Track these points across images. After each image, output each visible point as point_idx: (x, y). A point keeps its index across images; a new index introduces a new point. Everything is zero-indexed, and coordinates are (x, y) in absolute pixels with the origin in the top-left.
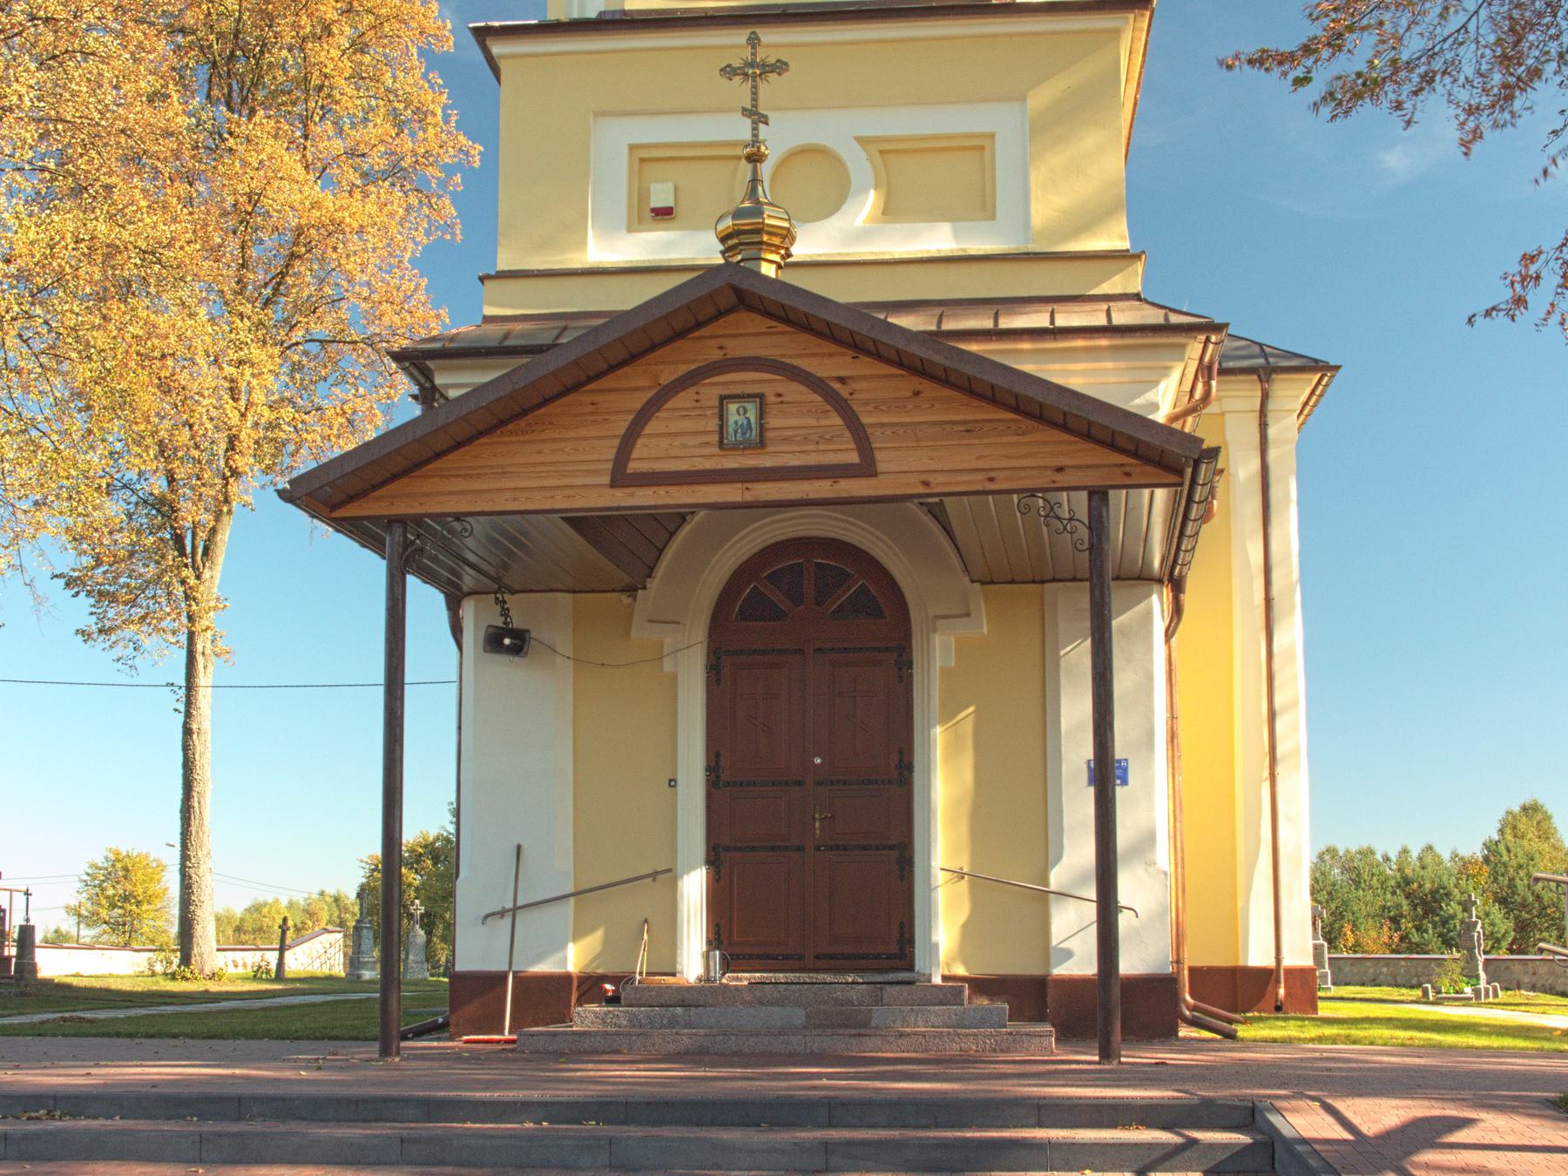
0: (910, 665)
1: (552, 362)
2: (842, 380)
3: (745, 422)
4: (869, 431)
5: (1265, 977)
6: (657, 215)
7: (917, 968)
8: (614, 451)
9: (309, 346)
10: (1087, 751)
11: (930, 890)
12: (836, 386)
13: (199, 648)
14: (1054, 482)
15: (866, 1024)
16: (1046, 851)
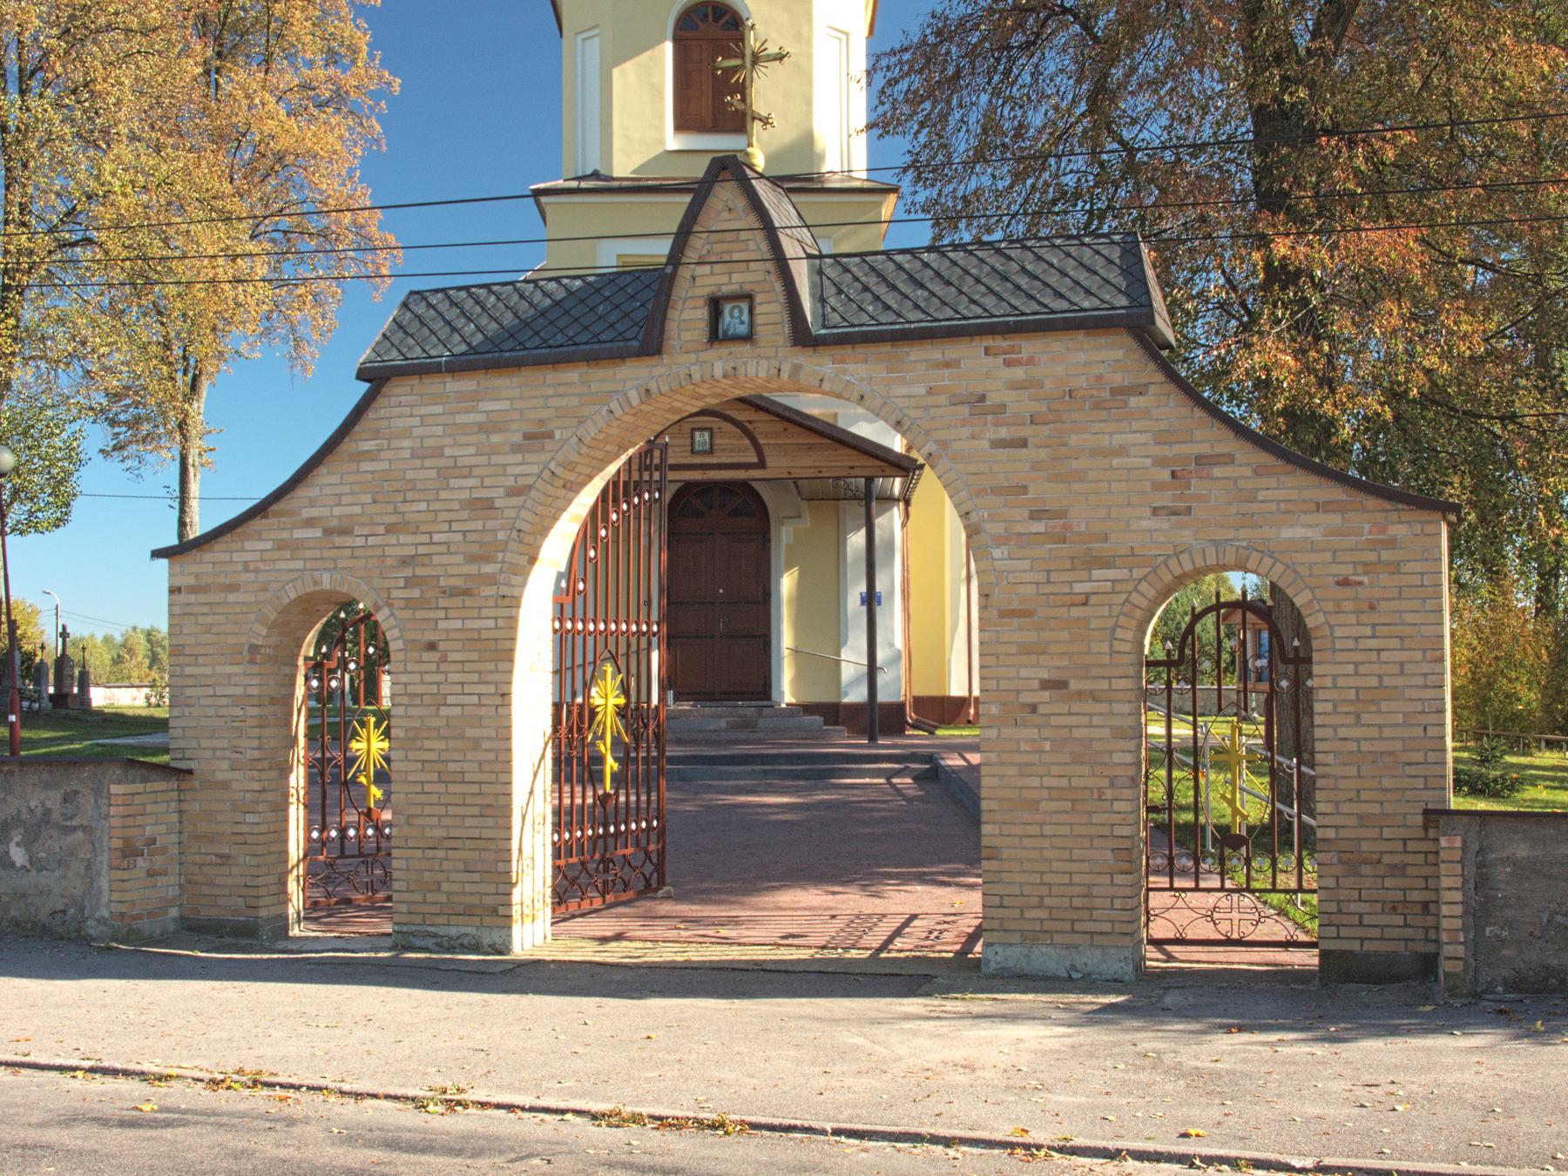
0: (769, 542)
2: (750, 422)
5: (962, 703)
9: (275, 235)
10: (863, 588)
11: (780, 659)
12: (747, 425)
13: (190, 461)
15: (755, 726)
16: (838, 642)
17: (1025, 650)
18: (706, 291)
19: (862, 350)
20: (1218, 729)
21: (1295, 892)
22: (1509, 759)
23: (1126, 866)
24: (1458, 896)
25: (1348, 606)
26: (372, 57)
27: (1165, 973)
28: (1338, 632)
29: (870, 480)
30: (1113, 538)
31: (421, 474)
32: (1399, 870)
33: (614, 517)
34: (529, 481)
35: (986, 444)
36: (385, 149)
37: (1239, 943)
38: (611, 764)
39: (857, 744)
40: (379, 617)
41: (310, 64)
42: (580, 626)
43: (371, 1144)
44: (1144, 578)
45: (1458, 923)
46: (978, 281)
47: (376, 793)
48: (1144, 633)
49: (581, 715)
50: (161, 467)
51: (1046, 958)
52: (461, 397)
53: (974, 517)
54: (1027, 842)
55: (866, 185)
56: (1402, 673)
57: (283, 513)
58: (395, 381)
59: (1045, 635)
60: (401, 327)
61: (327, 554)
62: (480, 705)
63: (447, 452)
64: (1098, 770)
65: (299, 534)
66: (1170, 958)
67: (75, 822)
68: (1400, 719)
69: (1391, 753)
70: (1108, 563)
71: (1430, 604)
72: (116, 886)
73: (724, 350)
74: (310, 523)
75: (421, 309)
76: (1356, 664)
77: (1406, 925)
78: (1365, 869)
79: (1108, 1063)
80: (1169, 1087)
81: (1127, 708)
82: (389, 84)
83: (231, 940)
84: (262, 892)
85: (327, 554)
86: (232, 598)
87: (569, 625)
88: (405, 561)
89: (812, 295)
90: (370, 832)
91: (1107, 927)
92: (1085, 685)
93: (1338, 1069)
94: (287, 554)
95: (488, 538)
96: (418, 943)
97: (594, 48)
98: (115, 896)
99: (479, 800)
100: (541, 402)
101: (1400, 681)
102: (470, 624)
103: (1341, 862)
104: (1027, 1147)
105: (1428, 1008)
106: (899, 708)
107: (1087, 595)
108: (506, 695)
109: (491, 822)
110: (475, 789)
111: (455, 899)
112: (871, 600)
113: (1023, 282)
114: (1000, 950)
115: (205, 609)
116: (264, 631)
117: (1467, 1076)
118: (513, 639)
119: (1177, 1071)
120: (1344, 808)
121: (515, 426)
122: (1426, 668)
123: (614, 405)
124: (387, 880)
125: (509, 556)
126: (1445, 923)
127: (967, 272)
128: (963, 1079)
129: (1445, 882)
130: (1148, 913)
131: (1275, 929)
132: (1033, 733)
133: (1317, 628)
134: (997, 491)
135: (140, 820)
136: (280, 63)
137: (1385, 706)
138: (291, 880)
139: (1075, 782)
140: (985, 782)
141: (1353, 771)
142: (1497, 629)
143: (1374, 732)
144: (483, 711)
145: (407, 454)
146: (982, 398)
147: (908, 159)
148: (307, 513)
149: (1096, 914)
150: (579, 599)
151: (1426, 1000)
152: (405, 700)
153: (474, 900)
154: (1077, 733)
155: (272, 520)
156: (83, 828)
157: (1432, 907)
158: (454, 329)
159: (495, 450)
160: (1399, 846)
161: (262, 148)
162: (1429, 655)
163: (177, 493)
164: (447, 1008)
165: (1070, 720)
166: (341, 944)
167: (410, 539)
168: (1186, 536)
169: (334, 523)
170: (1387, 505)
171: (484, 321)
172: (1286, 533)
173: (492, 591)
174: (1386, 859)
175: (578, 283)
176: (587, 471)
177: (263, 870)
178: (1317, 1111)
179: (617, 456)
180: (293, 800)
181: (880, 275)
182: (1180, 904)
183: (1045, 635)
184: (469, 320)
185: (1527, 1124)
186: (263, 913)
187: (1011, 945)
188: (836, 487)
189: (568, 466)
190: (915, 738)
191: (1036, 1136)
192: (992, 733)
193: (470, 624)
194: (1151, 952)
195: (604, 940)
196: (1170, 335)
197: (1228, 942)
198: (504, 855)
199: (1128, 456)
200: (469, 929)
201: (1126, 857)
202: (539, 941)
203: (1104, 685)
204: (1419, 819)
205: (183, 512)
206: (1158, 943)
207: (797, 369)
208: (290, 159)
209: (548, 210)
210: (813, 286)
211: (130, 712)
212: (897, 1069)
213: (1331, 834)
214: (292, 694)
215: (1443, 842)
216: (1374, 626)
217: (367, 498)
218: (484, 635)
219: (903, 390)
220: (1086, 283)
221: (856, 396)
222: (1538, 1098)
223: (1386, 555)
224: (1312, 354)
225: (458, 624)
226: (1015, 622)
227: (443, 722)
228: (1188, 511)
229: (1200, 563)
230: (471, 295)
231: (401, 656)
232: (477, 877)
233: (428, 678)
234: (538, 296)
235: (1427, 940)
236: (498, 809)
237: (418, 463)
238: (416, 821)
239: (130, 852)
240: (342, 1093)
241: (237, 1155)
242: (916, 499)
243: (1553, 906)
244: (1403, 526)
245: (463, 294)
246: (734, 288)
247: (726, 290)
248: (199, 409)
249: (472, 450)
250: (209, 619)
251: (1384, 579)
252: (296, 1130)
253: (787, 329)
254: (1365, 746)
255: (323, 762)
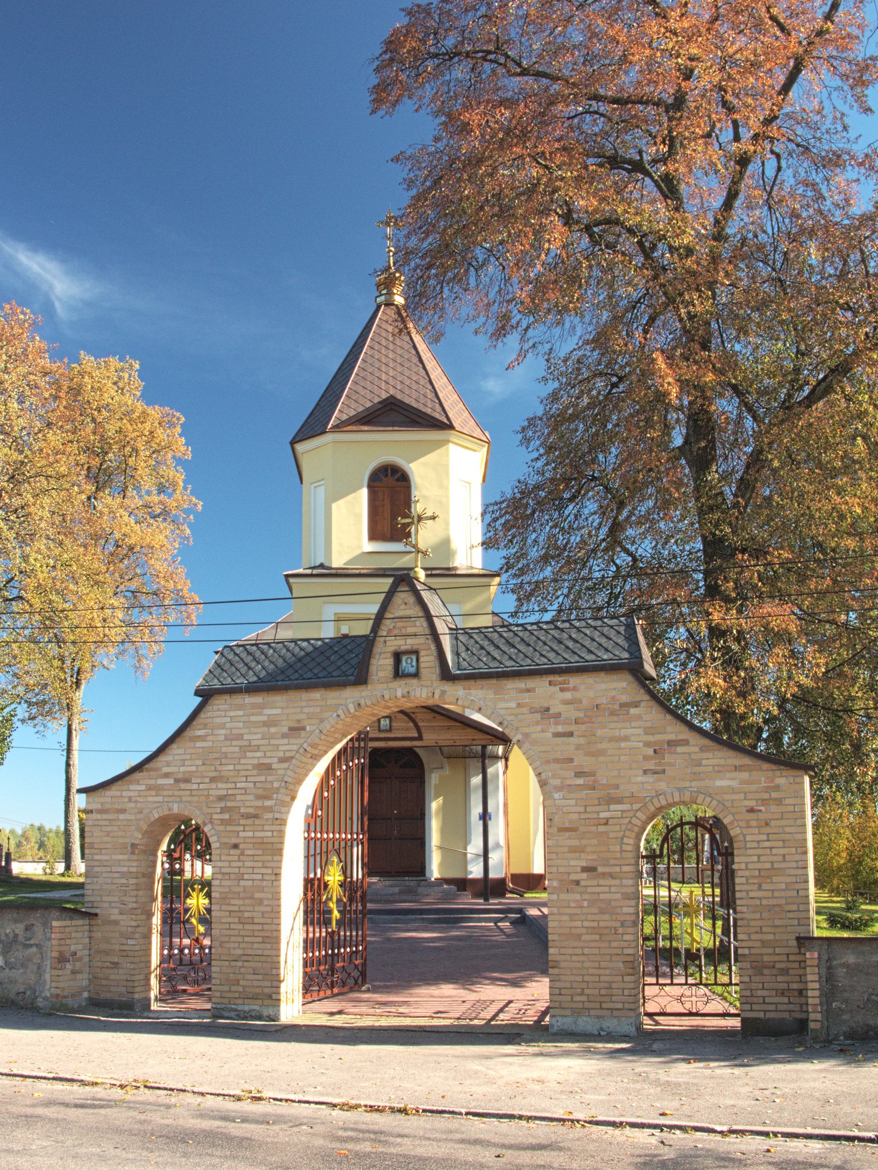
9: (127, 594)
10: (480, 810)
11: (431, 852)
16: (466, 841)
17: (573, 850)
18: (392, 649)
19: (480, 682)
20: (685, 892)
21: (728, 985)
22: (863, 907)
23: (631, 971)
24: (817, 985)
25: (754, 823)
26: (185, 489)
27: (654, 1032)
28: (748, 838)
29: (484, 747)
30: (622, 787)
31: (231, 749)
32: (785, 972)
33: (338, 773)
34: (292, 754)
35: (550, 735)
36: (191, 543)
37: (697, 1014)
38: (336, 914)
39: (479, 903)
40: (206, 829)
41: (149, 493)
42: (319, 835)
43: (214, 1118)
44: (639, 809)
45: (817, 1001)
46: (545, 643)
47: (202, 929)
48: (640, 840)
49: (319, 886)
50: (56, 731)
51: (586, 1023)
52: (254, 706)
53: (543, 776)
54: (574, 958)
55: (482, 572)
56: (784, 861)
57: (148, 770)
58: (216, 697)
59: (584, 842)
60: (219, 666)
61: (177, 793)
62: (263, 880)
63: (245, 737)
64: (614, 917)
65: (160, 781)
66: (657, 1023)
67: (32, 942)
68: (783, 886)
69: (779, 905)
70: (619, 801)
71: (799, 822)
72: (54, 978)
73: (402, 682)
74: (167, 775)
75: (231, 656)
76: (759, 856)
77: (790, 1003)
78: (766, 971)
79: (619, 1079)
80: (652, 1091)
81: (630, 882)
82: (195, 505)
83: (118, 1011)
84: (136, 984)
85: (177, 793)
86: (122, 817)
87: (313, 835)
88: (221, 798)
89: (452, 651)
90: (197, 951)
91: (620, 1006)
92: (607, 870)
93: (746, 1081)
94: (154, 793)
95: (268, 786)
96: (226, 1014)
97: (321, 491)
98: (53, 985)
99: (262, 934)
100: (299, 710)
101: (783, 865)
102: (258, 834)
103: (752, 967)
104: (572, 1121)
105: (801, 1049)
106: (502, 882)
107: (607, 819)
108: (278, 875)
109: (268, 946)
110: (260, 927)
111: (247, 989)
112: (485, 817)
113: (570, 644)
114: (560, 1019)
115: (106, 823)
116: (140, 836)
117: (817, 1084)
118: (282, 843)
119: (657, 1083)
120: (753, 937)
121: (284, 723)
122: (798, 857)
123: (340, 712)
124: (207, 979)
125: (280, 796)
126: (810, 1001)
127: (539, 639)
128: (537, 1087)
129: (810, 978)
130: (644, 997)
131: (717, 1006)
132: (578, 897)
133: (737, 836)
134: (556, 761)
135: (68, 941)
136: (130, 492)
137: (775, 879)
138: (153, 976)
139: (602, 924)
140: (550, 924)
141: (758, 916)
142: (863, 829)
143: (769, 894)
144: (265, 883)
145: (222, 738)
146: (548, 709)
147: (503, 561)
148: (166, 770)
149: (614, 998)
150: (318, 820)
151: (801, 1044)
152: (220, 876)
153: (259, 990)
154: (602, 896)
155: (145, 773)
156: (37, 945)
157: (804, 992)
158: (250, 668)
159: (273, 736)
160: (785, 958)
161: (120, 543)
162: (799, 850)
163: (65, 747)
164: (247, 1049)
165: (598, 889)
166: (179, 1014)
167: (224, 786)
168: (662, 786)
169: (180, 776)
170: (774, 767)
171: (267, 663)
172: (719, 783)
173: (270, 816)
174: (778, 965)
175: (320, 643)
176: (325, 748)
177: (137, 972)
178: (732, 1102)
179: (341, 740)
180: (154, 931)
181: (490, 640)
182: (663, 993)
183: (584, 842)
184: (258, 663)
185: (846, 1108)
186: (137, 996)
187: (565, 1016)
188: (464, 751)
189: (314, 746)
190: (511, 899)
191: (576, 1116)
192: (554, 897)
193: (258, 834)
194: (646, 1020)
195: (332, 1014)
196: (653, 673)
197: (690, 1014)
198: (276, 965)
199: (629, 741)
200: (254, 1006)
201: (631, 965)
202: (296, 1014)
203: (617, 869)
204: (795, 943)
205: (68, 758)
206: (650, 1015)
207: (443, 693)
208: (138, 549)
209: (294, 587)
210: (452, 646)
211: (35, 878)
212: (500, 1082)
213: (746, 951)
214: (154, 872)
215: (808, 955)
216: (768, 834)
217: (200, 762)
218: (265, 840)
219: (503, 705)
220: (605, 645)
221: (477, 708)
222: (854, 1095)
223: (774, 795)
224: (735, 678)
225: (250, 834)
226: (567, 834)
227: (241, 889)
228: (664, 771)
229: (670, 801)
230: (259, 648)
231: (218, 851)
232: (260, 977)
233: (233, 864)
234: (297, 650)
235: (802, 1011)
236: (273, 939)
237: (228, 743)
238: (228, 945)
239: (62, 959)
240: (194, 1092)
241: (142, 1122)
242: (512, 757)
243: (870, 990)
244: (783, 778)
245: (254, 648)
246: (408, 647)
247: (403, 648)
248: (79, 696)
249: (260, 736)
250: (109, 829)
251: (774, 808)
252: (172, 1111)
253: (438, 671)
254: (764, 902)
255: (172, 910)
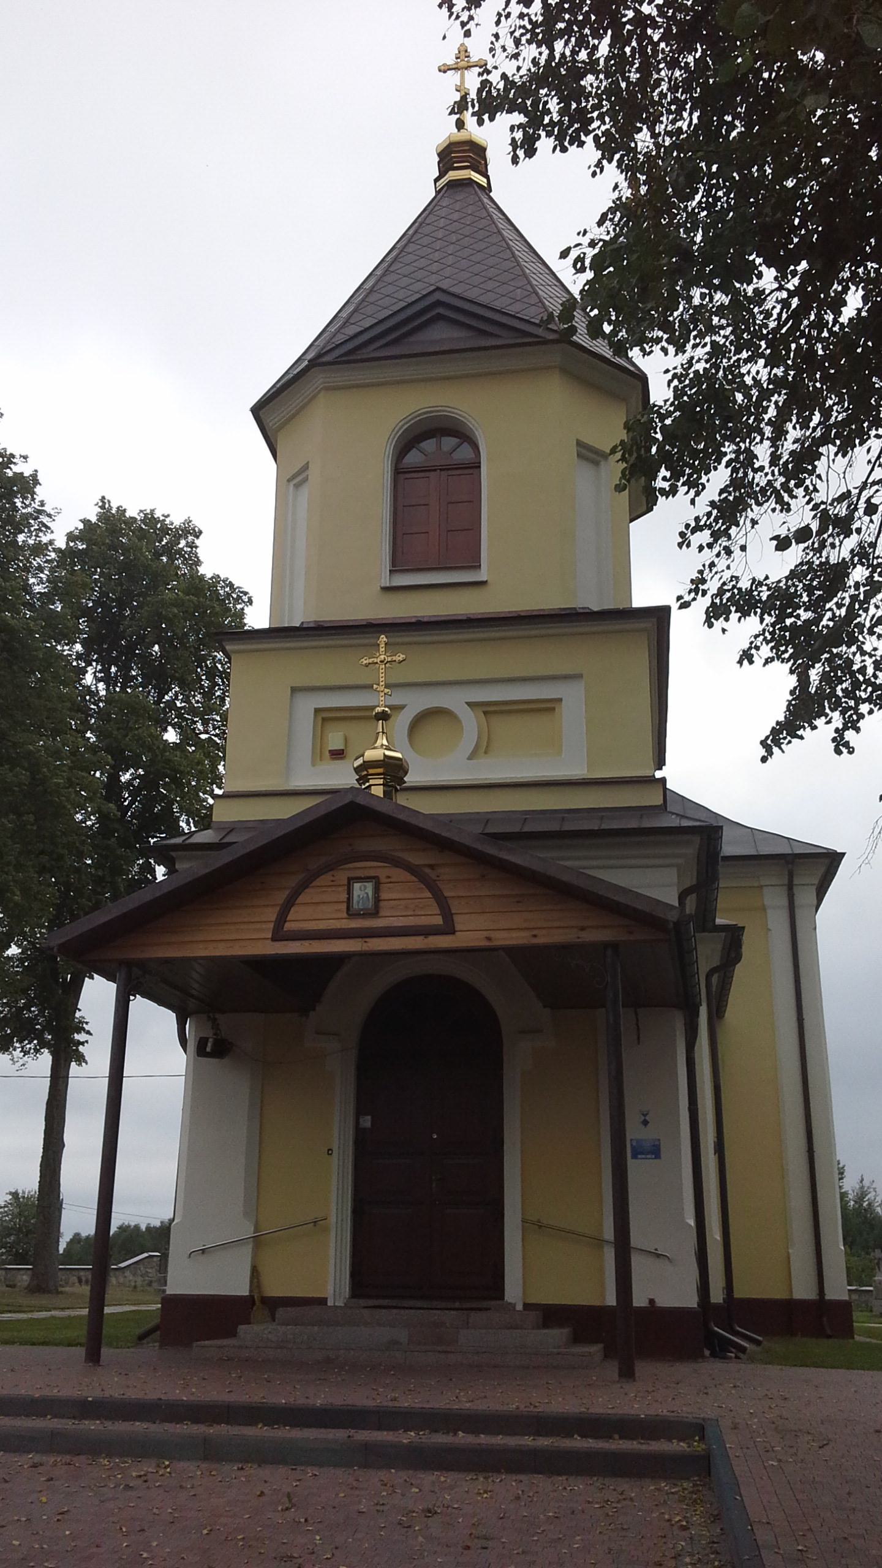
1: (224, 858)
2: (432, 867)
3: (365, 895)
4: (450, 902)
6: (333, 755)
7: (506, 1299)
8: (275, 916)
14: (579, 938)
